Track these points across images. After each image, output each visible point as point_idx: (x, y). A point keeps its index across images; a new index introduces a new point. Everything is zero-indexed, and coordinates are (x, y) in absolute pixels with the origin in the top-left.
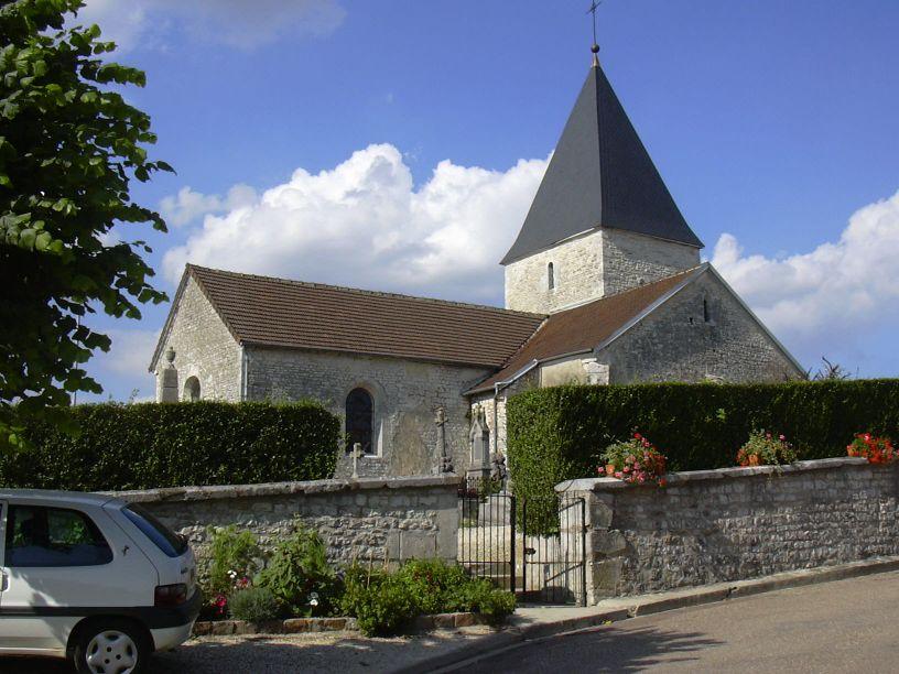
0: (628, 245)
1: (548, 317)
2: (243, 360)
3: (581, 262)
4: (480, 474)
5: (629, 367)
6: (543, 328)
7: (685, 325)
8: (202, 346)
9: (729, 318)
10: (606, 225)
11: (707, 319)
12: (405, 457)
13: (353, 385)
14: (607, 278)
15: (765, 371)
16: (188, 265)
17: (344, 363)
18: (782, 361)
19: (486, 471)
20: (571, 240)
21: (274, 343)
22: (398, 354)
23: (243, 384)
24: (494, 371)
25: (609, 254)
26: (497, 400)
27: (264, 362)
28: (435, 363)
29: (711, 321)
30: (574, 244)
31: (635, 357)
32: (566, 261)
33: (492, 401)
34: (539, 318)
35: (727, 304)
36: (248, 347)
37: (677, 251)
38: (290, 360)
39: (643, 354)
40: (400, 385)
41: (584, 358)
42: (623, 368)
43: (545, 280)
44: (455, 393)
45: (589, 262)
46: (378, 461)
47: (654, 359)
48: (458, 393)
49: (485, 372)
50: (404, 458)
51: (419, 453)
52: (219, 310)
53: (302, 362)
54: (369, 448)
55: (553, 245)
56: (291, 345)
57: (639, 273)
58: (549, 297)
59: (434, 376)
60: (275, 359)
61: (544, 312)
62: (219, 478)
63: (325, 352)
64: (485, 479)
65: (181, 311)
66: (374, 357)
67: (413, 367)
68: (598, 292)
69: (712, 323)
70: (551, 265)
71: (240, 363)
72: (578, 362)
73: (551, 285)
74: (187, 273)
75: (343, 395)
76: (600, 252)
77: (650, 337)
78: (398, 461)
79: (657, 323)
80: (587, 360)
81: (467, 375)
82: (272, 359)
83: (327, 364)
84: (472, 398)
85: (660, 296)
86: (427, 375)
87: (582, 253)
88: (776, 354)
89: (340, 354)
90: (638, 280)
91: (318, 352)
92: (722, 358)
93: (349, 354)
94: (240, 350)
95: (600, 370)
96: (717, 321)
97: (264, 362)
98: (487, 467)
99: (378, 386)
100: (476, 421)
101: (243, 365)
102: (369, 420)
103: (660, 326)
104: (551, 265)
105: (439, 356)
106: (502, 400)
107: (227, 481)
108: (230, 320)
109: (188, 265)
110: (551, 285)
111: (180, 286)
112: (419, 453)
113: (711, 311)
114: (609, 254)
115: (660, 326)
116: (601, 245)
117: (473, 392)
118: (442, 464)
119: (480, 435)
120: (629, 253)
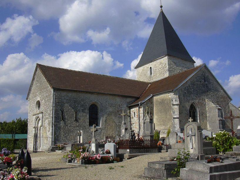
0: (175, 61)
1: (150, 83)
2: (53, 94)
3: (161, 66)
4: (149, 138)
5: (184, 96)
6: (150, 86)
7: (199, 83)
8: (41, 90)
9: (211, 81)
10: (169, 55)
11: (205, 82)
12: (109, 127)
13: (91, 103)
14: (169, 71)
15: (221, 98)
16: (37, 64)
17: (88, 96)
18: (225, 95)
19: (152, 137)
20: (157, 60)
21: (64, 88)
22: (106, 93)
23: (53, 103)
24: (137, 98)
25: (170, 63)
26: (139, 108)
27: (60, 95)
28: (119, 96)
29: (206, 82)
30: (158, 61)
31: (185, 93)
32: (156, 66)
33: (137, 108)
34: (148, 84)
35: (210, 77)
36: (55, 89)
37: (188, 64)
38: (70, 94)
39: (188, 92)
40: (107, 103)
41: (169, 93)
42: (182, 96)
43: (149, 72)
44: (125, 106)
45: (163, 66)
46: (100, 129)
47: (191, 94)
48: (126, 105)
49: (134, 99)
50: (109, 127)
51: (114, 126)
52: (46, 77)
53: (74, 95)
54: (97, 125)
55: (151, 62)
56: (70, 89)
57: (178, 70)
58: (150, 77)
59: (118, 100)
60: (64, 94)
61: (149, 82)
62: (55, 132)
63: (82, 91)
64: (151, 141)
65: (35, 79)
66: (99, 94)
67: (111, 97)
68: (167, 75)
69: (207, 83)
70: (151, 68)
71: (52, 95)
72: (167, 94)
73: (151, 74)
74: (37, 67)
75: (88, 106)
76: (167, 62)
77: (190, 87)
78: (106, 128)
79: (191, 82)
80: (170, 94)
81: (129, 100)
82: (64, 94)
83: (82, 96)
84: (130, 108)
85: (192, 73)
86: (116, 100)
87: (161, 63)
88: (224, 93)
89: (87, 92)
90: (178, 71)
91: (80, 92)
92: (209, 94)
93: (90, 93)
94: (52, 90)
95: (175, 97)
96: (207, 82)
97: (60, 95)
98: (152, 135)
99: (100, 103)
100: (146, 114)
101: (53, 96)
102: (97, 114)
103: (192, 83)
104: (151, 68)
105: (65, 170)
106: (141, 108)
107: (193, 84)
108: (49, 81)
109: (37, 64)
110: (151, 74)
111: (35, 71)
112: (114, 126)
113: (206, 79)
114: (170, 63)
115: (192, 83)
116: (167, 61)
117: (131, 105)
118: (130, 133)
119: (149, 120)
120: (175, 63)
